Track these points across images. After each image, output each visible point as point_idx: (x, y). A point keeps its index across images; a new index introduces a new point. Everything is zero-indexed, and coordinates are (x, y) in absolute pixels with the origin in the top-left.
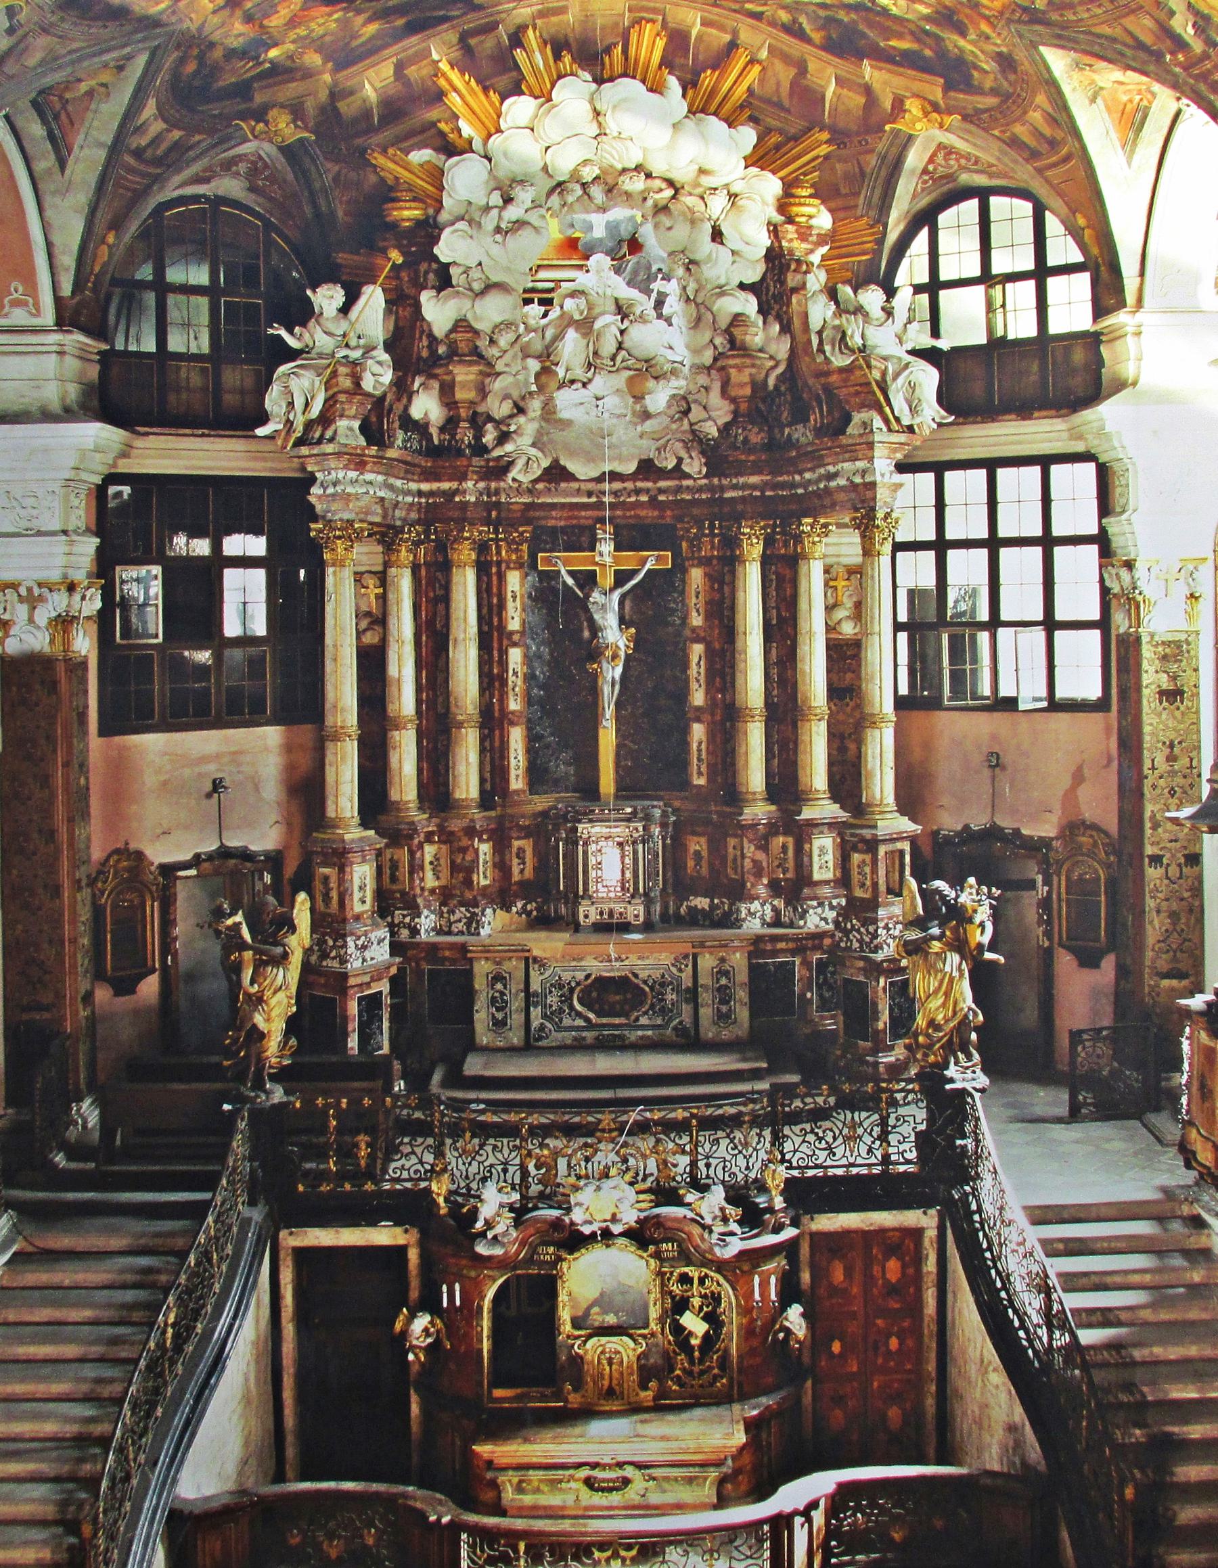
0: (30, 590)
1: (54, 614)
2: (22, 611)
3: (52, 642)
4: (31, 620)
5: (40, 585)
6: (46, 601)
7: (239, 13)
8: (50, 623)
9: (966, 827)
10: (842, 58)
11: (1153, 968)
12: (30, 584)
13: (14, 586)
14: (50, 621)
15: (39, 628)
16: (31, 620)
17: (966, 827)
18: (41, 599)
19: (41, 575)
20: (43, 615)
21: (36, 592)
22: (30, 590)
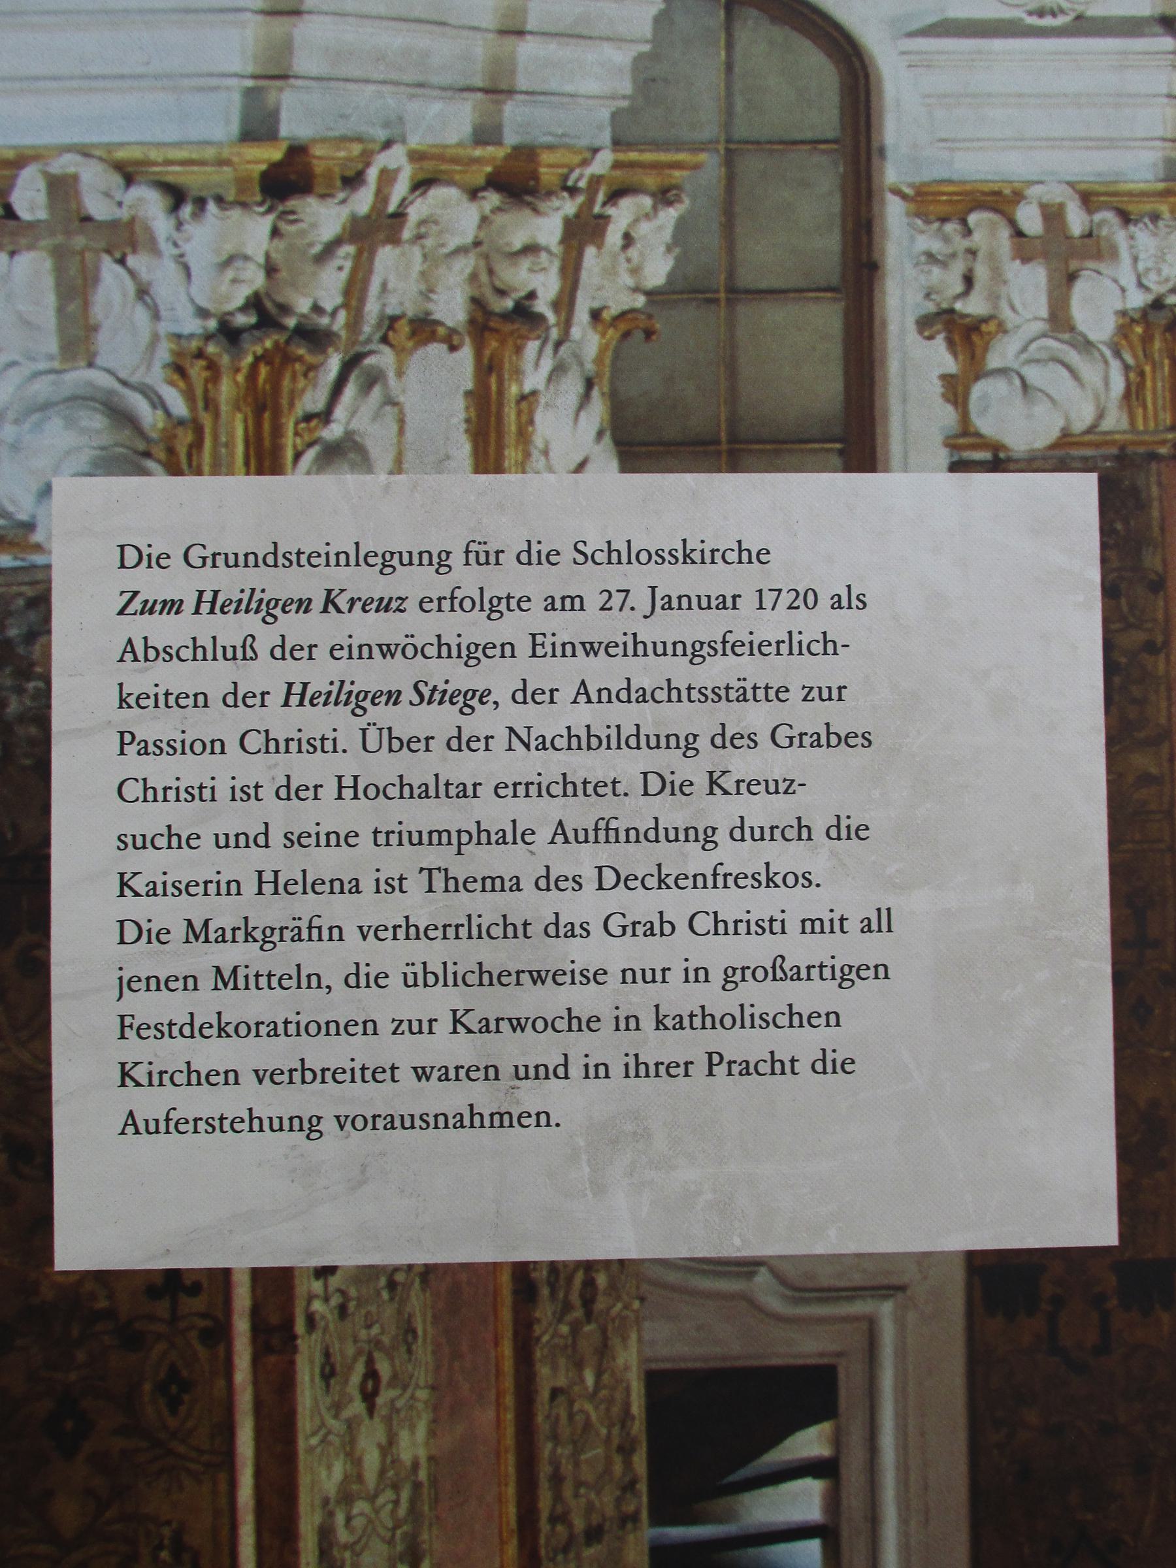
0: (1053, 215)
1: (1137, 300)
2: (1028, 286)
3: (1132, 395)
4: (1059, 320)
5: (1088, 199)
6: (1114, 254)
7: (59, 239)
8: (1123, 331)
9: (468, 394)
10: (358, 1267)
11: (719, 306)
12: (1056, 193)
13: (1000, 201)
14: (1127, 321)
15: (1086, 346)
16: (1059, 320)
17: (468, 394)
18: (1094, 247)
19: (1091, 166)
20: (1099, 304)
21: (1076, 221)
22: (1053, 215)
